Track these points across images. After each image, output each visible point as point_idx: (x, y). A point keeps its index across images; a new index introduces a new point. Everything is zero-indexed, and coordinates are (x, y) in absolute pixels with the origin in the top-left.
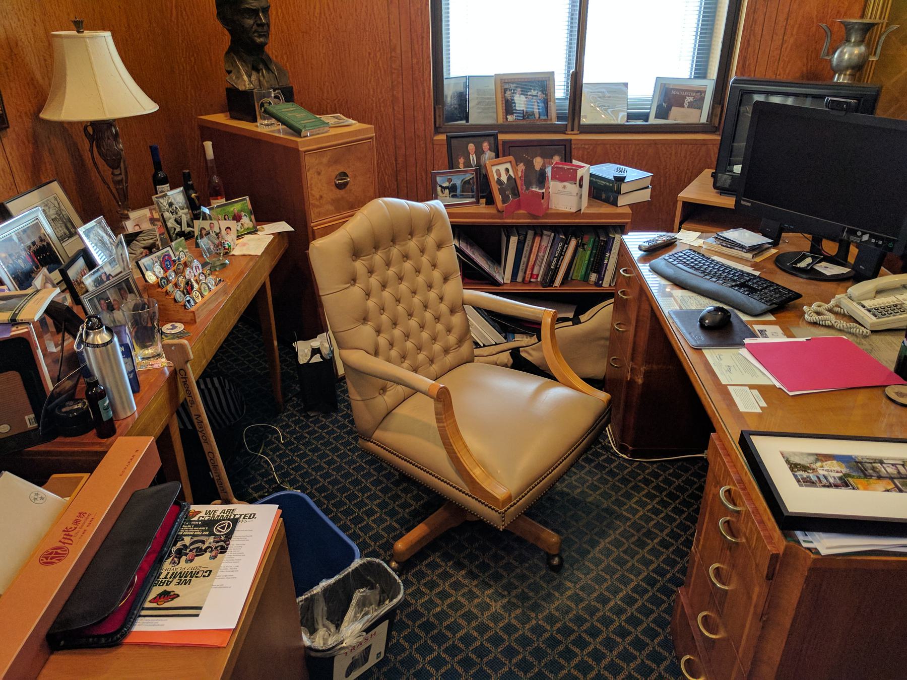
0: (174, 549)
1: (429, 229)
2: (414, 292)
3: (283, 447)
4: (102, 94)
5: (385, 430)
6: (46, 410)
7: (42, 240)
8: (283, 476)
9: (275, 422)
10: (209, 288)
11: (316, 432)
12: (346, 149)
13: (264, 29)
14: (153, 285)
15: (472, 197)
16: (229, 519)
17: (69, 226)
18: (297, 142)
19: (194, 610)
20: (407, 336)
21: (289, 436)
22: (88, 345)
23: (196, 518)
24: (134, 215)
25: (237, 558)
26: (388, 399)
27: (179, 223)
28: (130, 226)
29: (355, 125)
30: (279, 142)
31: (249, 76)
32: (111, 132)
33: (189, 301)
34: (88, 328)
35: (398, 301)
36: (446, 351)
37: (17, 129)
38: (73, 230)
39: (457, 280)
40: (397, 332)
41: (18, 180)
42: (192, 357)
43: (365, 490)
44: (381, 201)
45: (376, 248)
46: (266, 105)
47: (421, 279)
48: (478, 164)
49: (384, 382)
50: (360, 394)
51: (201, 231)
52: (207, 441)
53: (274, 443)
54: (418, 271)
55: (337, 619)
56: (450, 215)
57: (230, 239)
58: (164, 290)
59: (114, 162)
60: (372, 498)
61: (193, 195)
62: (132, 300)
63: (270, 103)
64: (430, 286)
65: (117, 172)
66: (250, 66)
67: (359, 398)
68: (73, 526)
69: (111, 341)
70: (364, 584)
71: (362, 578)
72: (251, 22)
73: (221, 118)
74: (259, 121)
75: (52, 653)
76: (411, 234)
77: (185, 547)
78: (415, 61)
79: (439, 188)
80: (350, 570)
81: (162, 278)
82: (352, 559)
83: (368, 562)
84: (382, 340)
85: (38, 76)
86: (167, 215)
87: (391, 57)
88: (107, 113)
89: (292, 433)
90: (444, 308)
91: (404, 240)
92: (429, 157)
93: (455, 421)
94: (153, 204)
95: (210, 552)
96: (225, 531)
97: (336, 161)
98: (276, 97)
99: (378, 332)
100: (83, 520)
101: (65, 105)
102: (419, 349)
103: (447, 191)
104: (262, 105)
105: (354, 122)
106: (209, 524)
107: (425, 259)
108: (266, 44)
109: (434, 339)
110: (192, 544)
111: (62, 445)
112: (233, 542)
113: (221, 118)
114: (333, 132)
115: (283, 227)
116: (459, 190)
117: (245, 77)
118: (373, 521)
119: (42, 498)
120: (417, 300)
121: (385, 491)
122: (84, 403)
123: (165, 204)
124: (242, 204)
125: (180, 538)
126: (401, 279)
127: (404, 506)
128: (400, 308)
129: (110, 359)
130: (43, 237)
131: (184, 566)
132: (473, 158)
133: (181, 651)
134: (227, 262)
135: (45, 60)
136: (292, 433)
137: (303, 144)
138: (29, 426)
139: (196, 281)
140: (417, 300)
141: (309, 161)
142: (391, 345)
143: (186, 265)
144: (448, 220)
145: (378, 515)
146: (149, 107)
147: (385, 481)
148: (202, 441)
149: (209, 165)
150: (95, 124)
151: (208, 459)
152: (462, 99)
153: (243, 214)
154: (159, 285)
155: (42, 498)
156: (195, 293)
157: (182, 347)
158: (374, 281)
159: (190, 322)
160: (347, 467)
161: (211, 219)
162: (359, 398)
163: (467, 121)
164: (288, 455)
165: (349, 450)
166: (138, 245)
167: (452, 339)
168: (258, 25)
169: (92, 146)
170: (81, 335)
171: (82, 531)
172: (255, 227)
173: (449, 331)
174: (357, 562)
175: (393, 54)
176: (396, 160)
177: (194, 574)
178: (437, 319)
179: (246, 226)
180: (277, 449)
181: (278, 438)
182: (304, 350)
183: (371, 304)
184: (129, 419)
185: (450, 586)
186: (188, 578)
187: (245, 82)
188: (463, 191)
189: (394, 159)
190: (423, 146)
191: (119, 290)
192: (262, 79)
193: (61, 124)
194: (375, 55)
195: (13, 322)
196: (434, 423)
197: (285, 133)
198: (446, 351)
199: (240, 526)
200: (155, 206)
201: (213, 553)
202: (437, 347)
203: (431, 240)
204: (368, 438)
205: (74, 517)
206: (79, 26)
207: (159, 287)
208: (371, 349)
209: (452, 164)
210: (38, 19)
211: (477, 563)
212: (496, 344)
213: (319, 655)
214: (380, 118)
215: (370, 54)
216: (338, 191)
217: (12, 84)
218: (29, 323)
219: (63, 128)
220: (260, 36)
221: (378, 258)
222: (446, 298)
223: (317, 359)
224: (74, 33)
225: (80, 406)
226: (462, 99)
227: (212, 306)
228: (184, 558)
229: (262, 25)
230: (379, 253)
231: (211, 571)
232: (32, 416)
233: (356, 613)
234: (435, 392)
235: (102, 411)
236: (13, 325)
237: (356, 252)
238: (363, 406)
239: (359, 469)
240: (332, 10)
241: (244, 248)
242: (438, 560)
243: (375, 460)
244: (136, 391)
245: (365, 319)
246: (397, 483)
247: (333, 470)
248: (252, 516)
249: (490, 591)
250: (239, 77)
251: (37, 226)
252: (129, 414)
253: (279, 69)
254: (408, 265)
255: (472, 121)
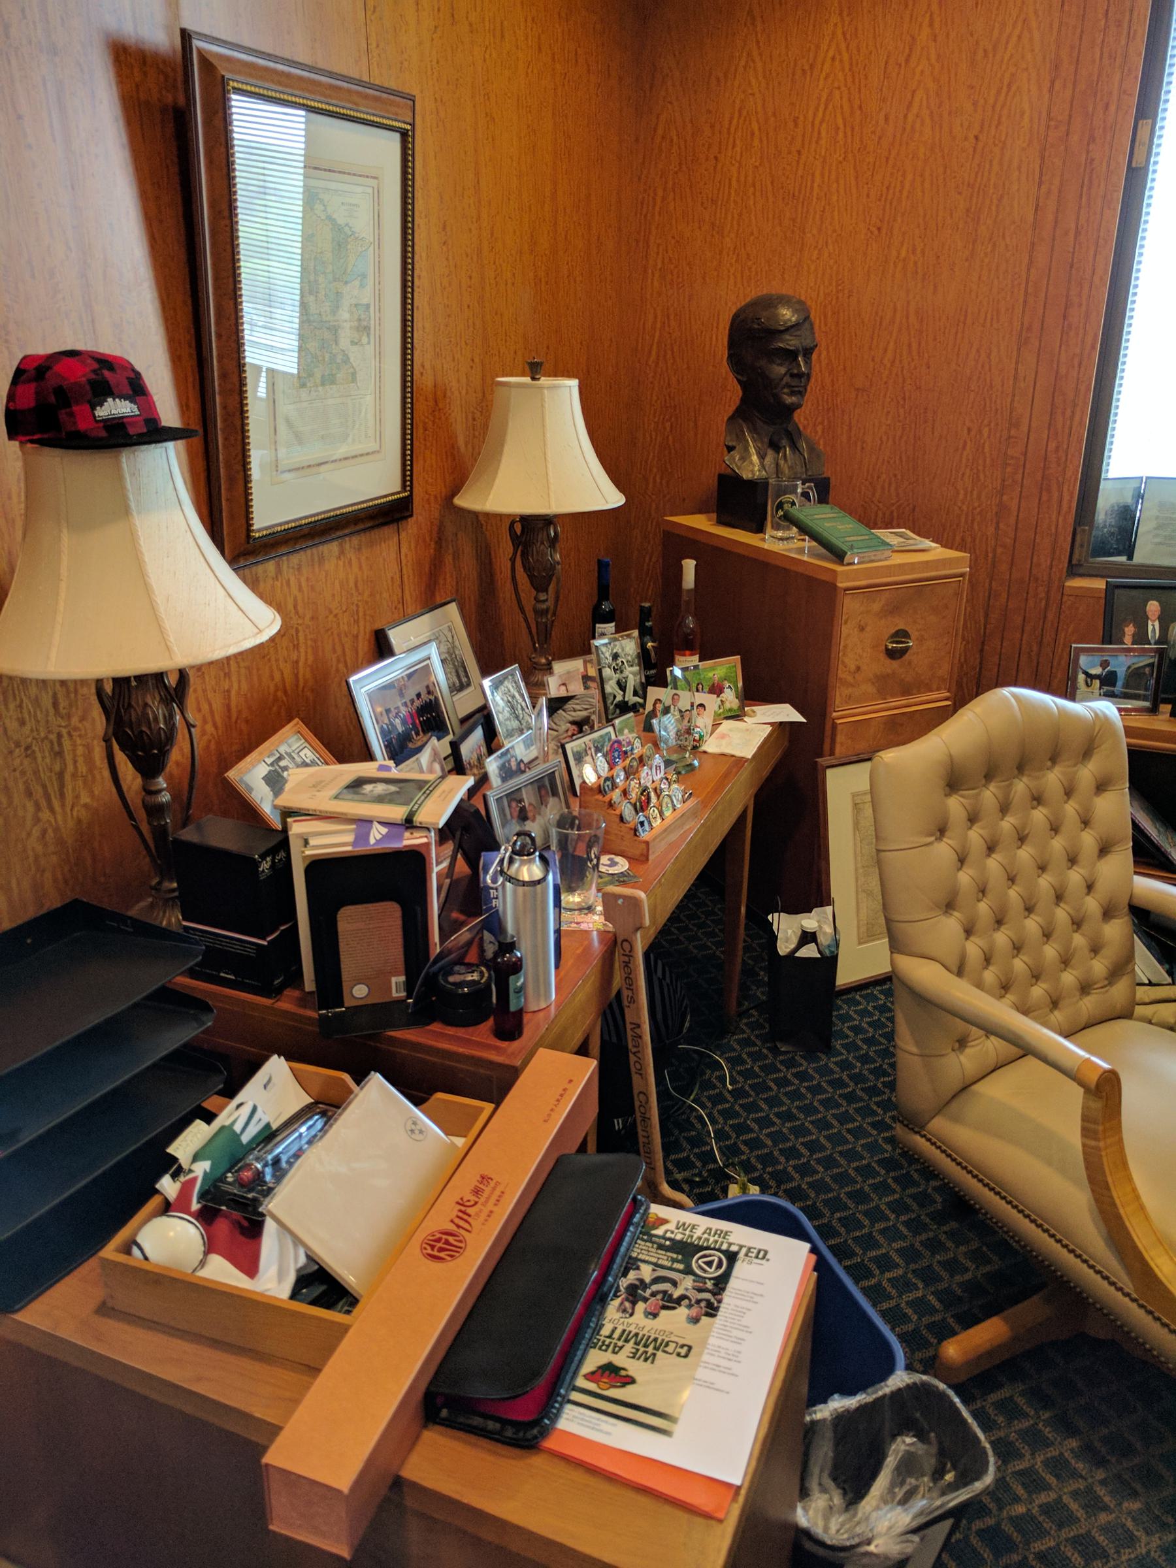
0: (624, 1283)
1: (1087, 753)
2: (1042, 868)
3: (728, 1096)
4: (550, 474)
5: (956, 1119)
6: (427, 973)
7: (429, 693)
8: (730, 1152)
9: (718, 1047)
10: (674, 806)
11: (789, 1083)
12: (914, 592)
13: (800, 381)
14: (591, 789)
15: (1145, 698)
16: (719, 1250)
17: (462, 674)
18: (835, 571)
19: (656, 1419)
20: (1017, 948)
21: (741, 1079)
22: (510, 879)
23: (659, 1232)
24: (560, 667)
25: (740, 1334)
26: (967, 1061)
27: (622, 686)
28: (554, 687)
29: (934, 551)
30: (800, 570)
31: (762, 457)
32: (548, 534)
33: (642, 824)
34: (514, 852)
35: (1012, 879)
36: (1085, 988)
37: (420, 518)
38: (464, 680)
39: (1123, 856)
40: (1001, 938)
41: (407, 596)
42: (647, 922)
43: (875, 1215)
44: (1007, 692)
45: (989, 777)
46: (786, 506)
47: (1058, 844)
48: (1163, 639)
49: (964, 1027)
50: (917, 1044)
51: (654, 705)
52: (641, 1073)
53: (715, 1087)
54: (1055, 829)
55: (854, 1483)
56: (1129, 732)
57: (702, 722)
58: (607, 799)
59: (541, 579)
60: (891, 1234)
61: (650, 644)
62: (552, 810)
63: (793, 503)
64: (1072, 861)
65: (543, 597)
66: (766, 440)
67: (914, 1050)
68: (473, 1198)
69: (544, 879)
70: (906, 1425)
71: (911, 1411)
72: (783, 370)
73: (702, 523)
74: (769, 531)
75: (425, 1426)
76: (1054, 759)
77: (643, 1284)
78: (1052, 445)
79: (1081, 677)
80: (887, 1390)
81: (607, 779)
82: (890, 1370)
83: (924, 1384)
84: (973, 949)
85: (461, 442)
86: (607, 672)
87: (1010, 437)
88: (553, 504)
89: (748, 1074)
90: (1092, 905)
91: (1041, 769)
92: (1050, 616)
93: (1121, 1140)
94: (589, 652)
95: (690, 1306)
96: (713, 1272)
97: (893, 609)
98: (805, 495)
99: (969, 932)
100: (487, 1190)
101: (495, 487)
102: (1036, 976)
103: (1097, 683)
104: (780, 506)
105: (934, 545)
106: (685, 1250)
107: (1070, 809)
108: (799, 406)
109: (1065, 962)
110: (656, 1280)
111: (439, 1039)
112: (729, 1299)
113: (702, 523)
114: (898, 559)
115: (788, 713)
116: (1120, 683)
117: (755, 458)
118: (889, 1280)
119: (421, 1132)
120: (1045, 882)
121: (916, 1226)
122: (482, 974)
123: (607, 655)
124: (726, 668)
125: (632, 1263)
126: (1022, 839)
127: (952, 1266)
128: (1013, 894)
129: (535, 911)
130: (431, 688)
131: (639, 1321)
132: (1153, 628)
133: (643, 1500)
134: (696, 763)
135: (474, 419)
136: (748, 1074)
137: (845, 576)
138: (395, 994)
139: (655, 790)
140: (1045, 882)
141: (850, 606)
142: (987, 960)
143: (641, 761)
144: (1124, 741)
145: (900, 1272)
146: (614, 499)
147: (915, 1207)
148: (633, 1070)
149: (685, 597)
150: (527, 521)
151: (637, 1104)
152: (1126, 518)
153: (727, 684)
154: (600, 790)
155: (421, 1132)
156: (653, 812)
157: (634, 902)
158: (975, 836)
159: (639, 858)
160: (843, 1162)
161: (676, 688)
162: (914, 1050)
163: (1130, 557)
164: (738, 1115)
165: (849, 1131)
166: (565, 716)
167: (1099, 967)
168: (792, 376)
169: (515, 554)
170: (502, 860)
171: (486, 1211)
172: (742, 707)
173: (1095, 950)
174: (899, 1379)
175: (1013, 432)
176: (986, 616)
177: (660, 1345)
178: (1077, 924)
179: (727, 706)
180: (718, 1099)
181: (722, 1079)
182: (787, 928)
183: (965, 878)
184: (541, 1014)
185: (1046, 1463)
186: (650, 1350)
187: (752, 465)
188: (1127, 685)
189: (982, 614)
190: (1043, 595)
191: (539, 788)
192: (782, 462)
193: (476, 514)
194: (980, 432)
195: (409, 823)
196: (1074, 1138)
197: (812, 553)
198: (1085, 988)
199: (740, 1268)
200: (593, 657)
201: (694, 1311)
202: (1069, 978)
203: (1087, 773)
204: (916, 1124)
205: (474, 1182)
206: (535, 370)
207: (600, 792)
208: (953, 963)
209: (1110, 635)
210: (477, 360)
211: (1105, 1431)
212: (1150, 984)
213: (821, 1552)
214: (969, 540)
215: (969, 430)
216: (888, 661)
217: (428, 453)
218: (428, 829)
219: (478, 521)
220: (792, 393)
221: (989, 795)
222: (1100, 887)
223: (809, 951)
224: (527, 380)
225: (475, 976)
226: (1126, 518)
227: (673, 837)
228: (640, 1306)
229: (800, 376)
230: (992, 787)
231: (690, 1348)
232: (402, 978)
233: (893, 1485)
234: (1093, 1078)
235: (512, 995)
236: (407, 828)
237: (954, 780)
238: (920, 1069)
239: (866, 1172)
240: (915, 353)
241: (724, 742)
242: (1021, 1401)
243: (913, 1171)
244: (557, 967)
245: (949, 906)
246: (940, 1218)
247: (819, 1161)
248: (762, 1255)
249: (1135, 1506)
250: (745, 457)
251: (427, 670)
252: (543, 1006)
253: (812, 449)
254: (1039, 815)
255: (1139, 558)
